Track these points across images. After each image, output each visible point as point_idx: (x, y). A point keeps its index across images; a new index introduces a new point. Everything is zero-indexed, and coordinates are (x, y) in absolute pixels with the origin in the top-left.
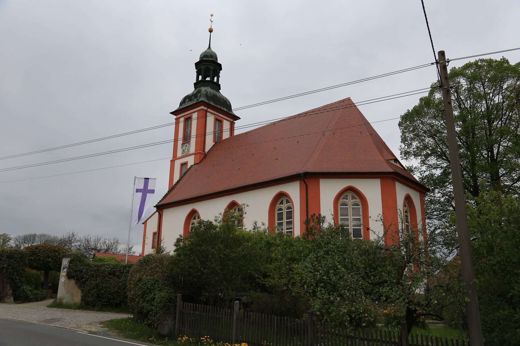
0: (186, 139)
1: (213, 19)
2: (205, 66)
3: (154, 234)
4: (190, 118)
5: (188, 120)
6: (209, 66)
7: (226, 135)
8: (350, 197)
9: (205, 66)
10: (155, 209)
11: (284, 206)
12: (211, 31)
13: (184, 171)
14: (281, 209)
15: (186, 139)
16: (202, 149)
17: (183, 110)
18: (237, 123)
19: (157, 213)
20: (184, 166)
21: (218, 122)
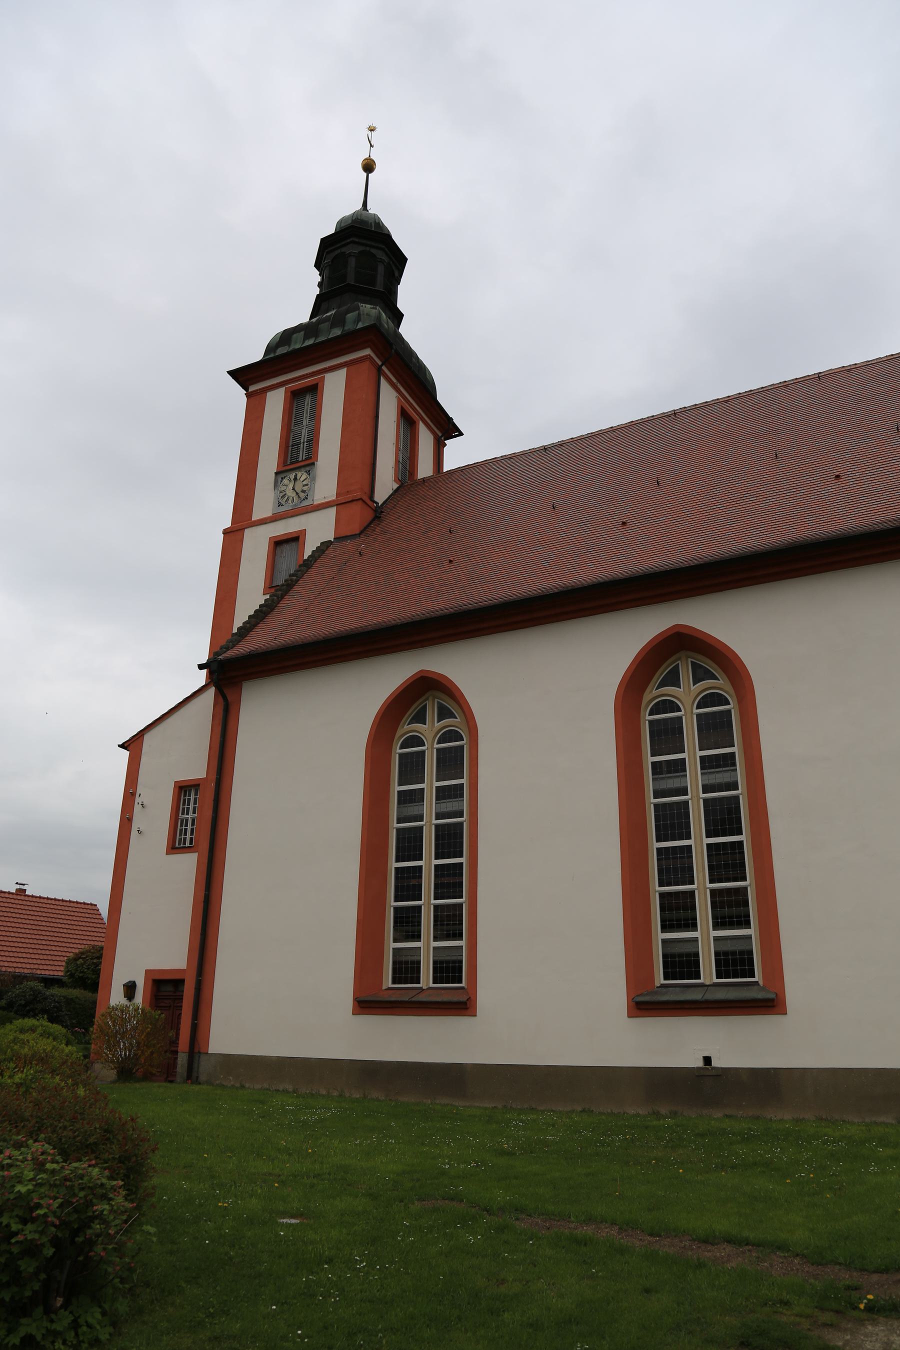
0: (297, 457)
1: (374, 136)
2: (361, 248)
3: (183, 789)
4: (314, 390)
5: (305, 397)
6: (373, 251)
7: (425, 469)
8: (686, 674)
9: (361, 248)
10: (201, 677)
11: (429, 730)
12: (369, 167)
13: (288, 564)
14: (416, 741)
15: (297, 457)
16: (367, 489)
17: (280, 369)
18: (451, 445)
19: (212, 690)
20: (286, 548)
21: (407, 420)
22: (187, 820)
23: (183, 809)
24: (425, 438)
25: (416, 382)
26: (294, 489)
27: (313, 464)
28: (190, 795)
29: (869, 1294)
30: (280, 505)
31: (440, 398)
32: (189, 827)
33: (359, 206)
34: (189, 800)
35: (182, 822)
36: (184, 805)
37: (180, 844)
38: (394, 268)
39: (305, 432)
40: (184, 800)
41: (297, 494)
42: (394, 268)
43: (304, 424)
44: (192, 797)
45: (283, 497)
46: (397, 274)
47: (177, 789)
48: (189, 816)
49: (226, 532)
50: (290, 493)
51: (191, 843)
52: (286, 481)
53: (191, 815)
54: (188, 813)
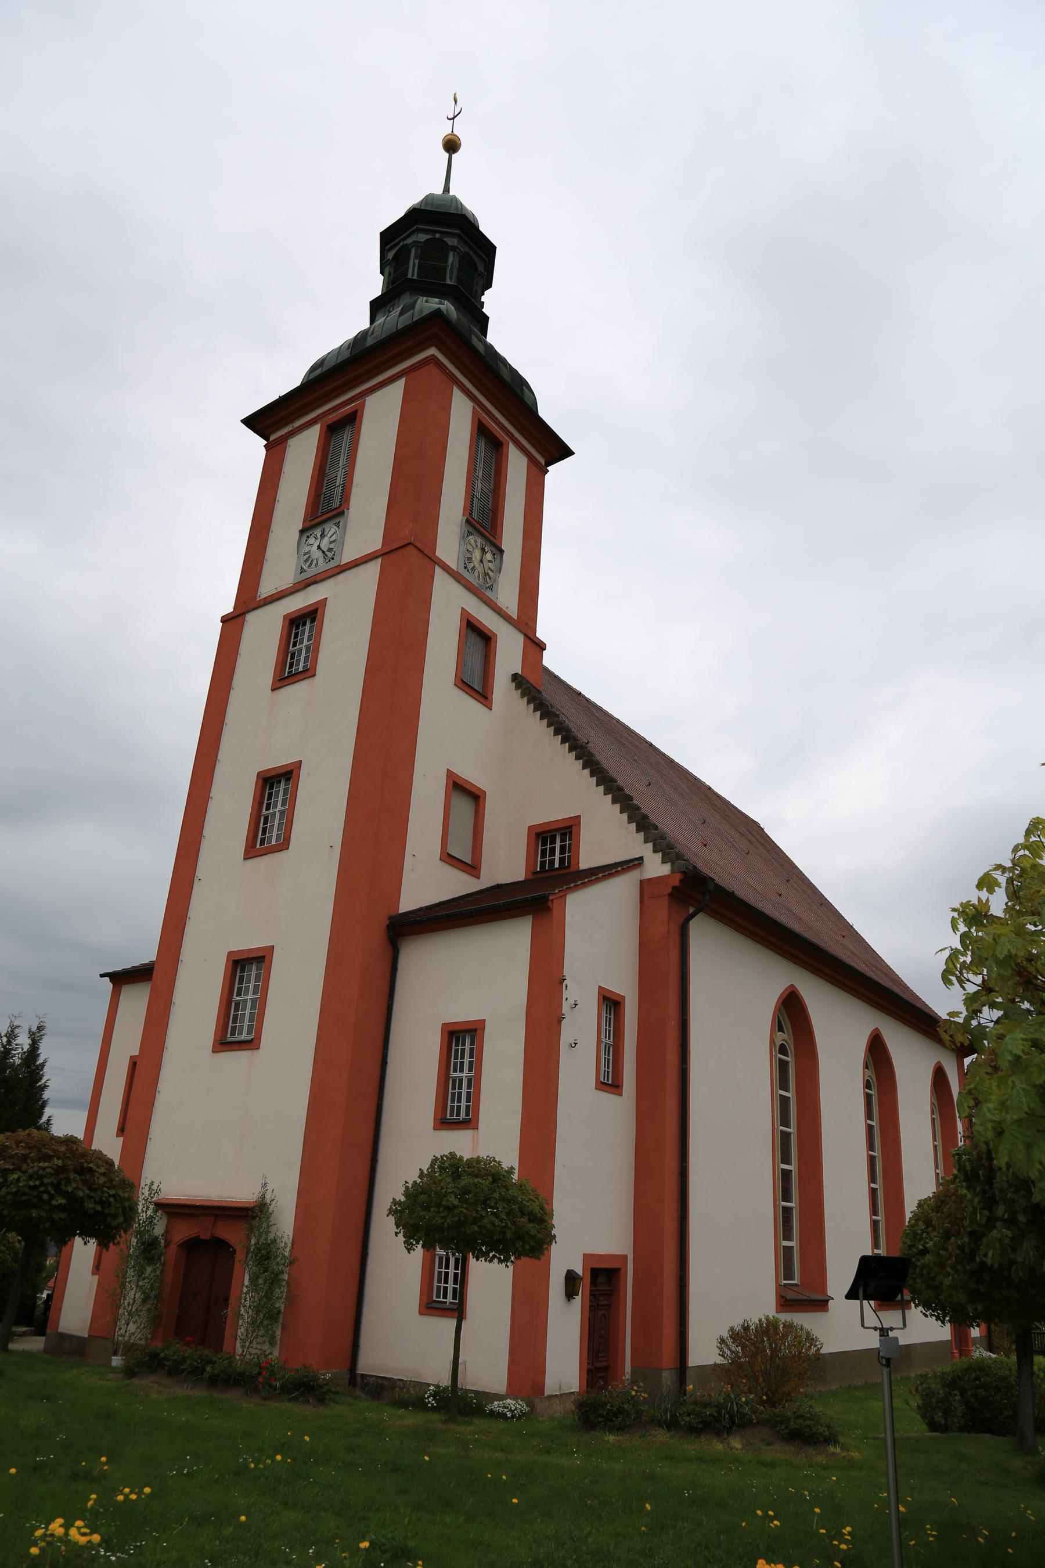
0: (326, 507)
2: (467, 250)
4: (353, 419)
5: (347, 423)
9: (467, 250)
12: (451, 146)
15: (326, 507)
21: (488, 442)
22: (461, 1081)
23: (455, 1064)
24: (516, 464)
25: (507, 395)
26: (319, 547)
27: (343, 513)
28: (464, 1044)
29: (367, 1550)
30: (302, 571)
31: (542, 413)
32: (464, 1091)
33: (439, 191)
34: (463, 1050)
35: (454, 1082)
36: (456, 1058)
37: (452, 1114)
38: (474, 257)
39: (340, 475)
40: (457, 1051)
41: (323, 552)
42: (474, 257)
43: (341, 464)
44: (467, 1047)
45: (306, 561)
46: (481, 267)
47: (446, 1035)
48: (464, 1075)
49: (225, 620)
50: (316, 554)
51: (467, 1114)
52: (311, 540)
53: (466, 1073)
54: (462, 1071)
